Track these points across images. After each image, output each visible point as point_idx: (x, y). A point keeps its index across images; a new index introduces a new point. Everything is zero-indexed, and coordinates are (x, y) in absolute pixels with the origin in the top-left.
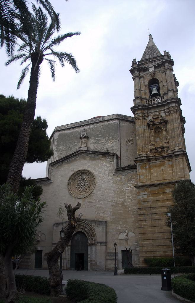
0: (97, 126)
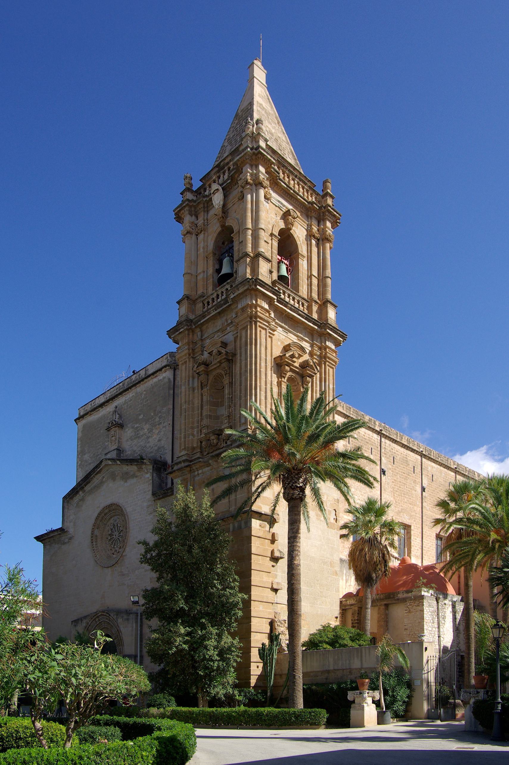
0: (136, 393)
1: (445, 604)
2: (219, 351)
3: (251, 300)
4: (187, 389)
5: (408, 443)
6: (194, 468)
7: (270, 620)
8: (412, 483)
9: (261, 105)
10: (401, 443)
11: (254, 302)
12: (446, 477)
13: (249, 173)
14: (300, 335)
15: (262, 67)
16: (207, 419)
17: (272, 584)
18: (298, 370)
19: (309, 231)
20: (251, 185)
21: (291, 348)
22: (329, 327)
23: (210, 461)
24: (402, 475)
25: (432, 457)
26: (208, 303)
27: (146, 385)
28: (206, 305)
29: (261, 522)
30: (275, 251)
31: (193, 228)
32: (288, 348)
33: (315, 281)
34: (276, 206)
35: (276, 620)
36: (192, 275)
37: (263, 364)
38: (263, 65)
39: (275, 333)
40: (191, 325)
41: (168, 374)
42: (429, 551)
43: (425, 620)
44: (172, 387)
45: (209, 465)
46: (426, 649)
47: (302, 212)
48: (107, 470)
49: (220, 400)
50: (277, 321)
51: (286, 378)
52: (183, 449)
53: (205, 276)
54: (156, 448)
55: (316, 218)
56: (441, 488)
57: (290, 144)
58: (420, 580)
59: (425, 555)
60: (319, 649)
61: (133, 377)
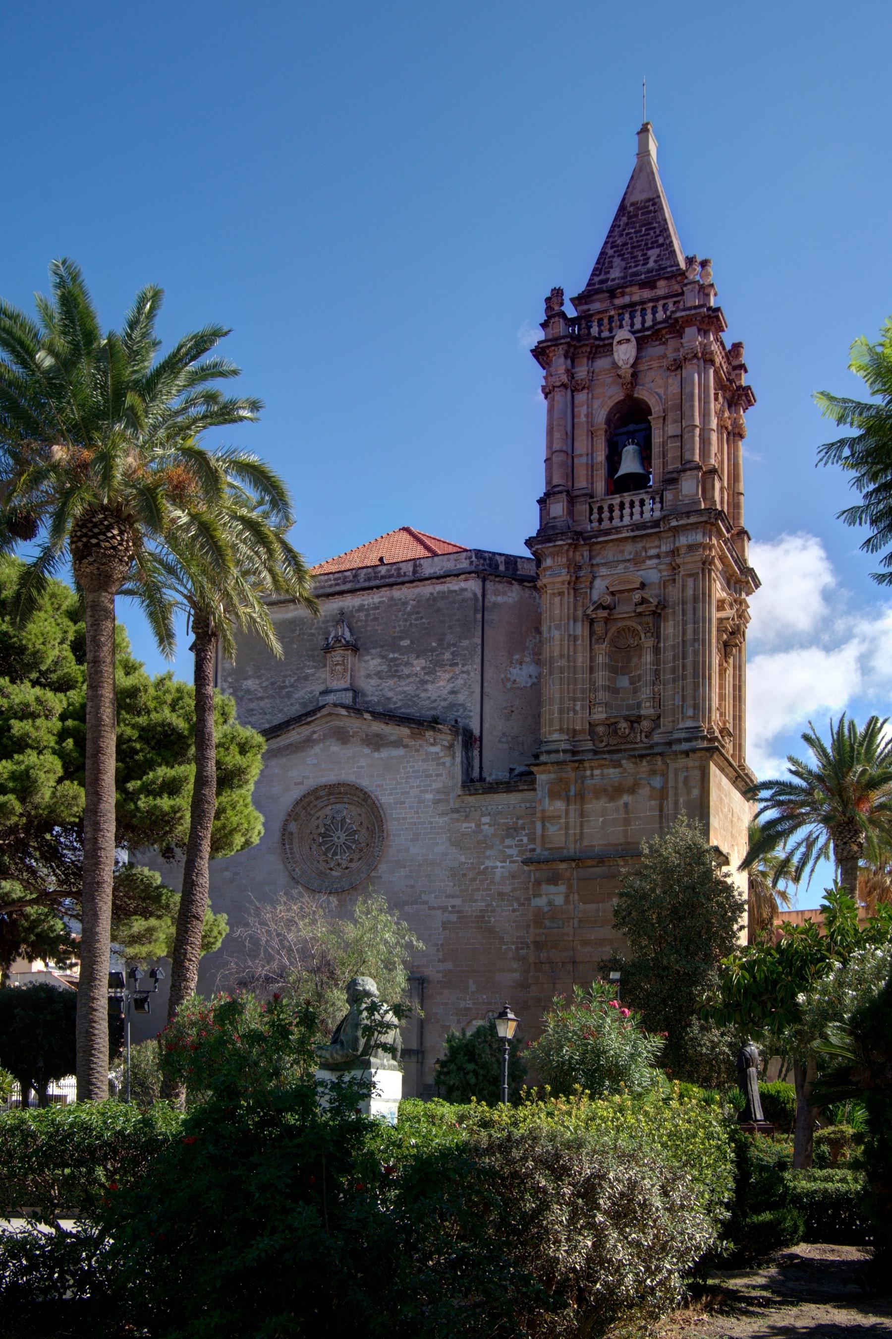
23: (624, 762)
26: (600, 509)
27: (417, 591)
28: (595, 510)
40: (578, 539)
41: (473, 585)
48: (327, 723)
49: (620, 665)
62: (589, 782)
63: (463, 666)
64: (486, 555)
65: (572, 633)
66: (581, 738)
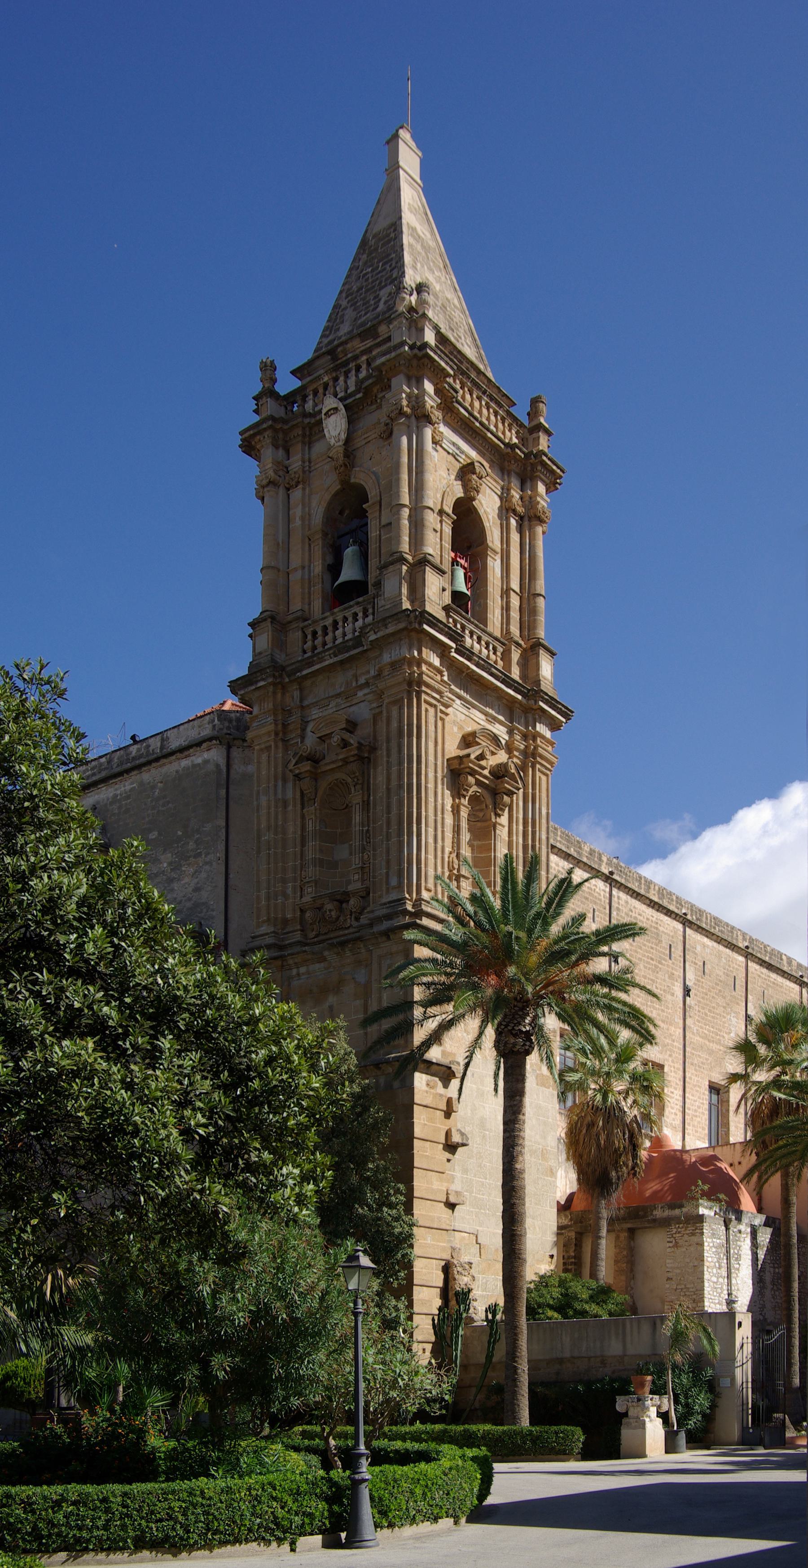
0: (142, 784)
1: (740, 1232)
2: (343, 740)
3: (410, 649)
4: (273, 803)
5: (659, 898)
6: (291, 962)
7: (443, 1263)
8: (667, 979)
9: (414, 229)
10: (647, 898)
11: (416, 653)
12: (729, 966)
13: (405, 392)
14: (490, 711)
15: (414, 144)
16: (315, 866)
17: (447, 1194)
18: (487, 782)
19: (505, 498)
20: (408, 416)
21: (477, 739)
22: (543, 697)
23: (326, 953)
24: (648, 963)
25: (704, 926)
26: (314, 634)
27: (164, 770)
28: (309, 637)
29: (429, 1077)
30: (447, 545)
31: (281, 473)
32: (471, 739)
33: (515, 601)
34: (449, 453)
35: (456, 1262)
36: (279, 570)
37: (431, 775)
38: (412, 137)
39: (449, 710)
40: (281, 676)
41: (214, 755)
42: (696, 1116)
43: (706, 1264)
44: (223, 782)
45: (323, 959)
46: (740, 1324)
47: (492, 461)
49: (339, 831)
50: (453, 687)
51: (467, 798)
52: (264, 922)
53: (307, 577)
54: (189, 904)
55: (518, 474)
56: (719, 988)
57: (467, 312)
58: (697, 1186)
59: (689, 1124)
60: (539, 1319)
61: (131, 749)
62: (295, 983)
63: (207, 854)
64: (233, 715)
65: (280, 797)
66: (291, 929)
